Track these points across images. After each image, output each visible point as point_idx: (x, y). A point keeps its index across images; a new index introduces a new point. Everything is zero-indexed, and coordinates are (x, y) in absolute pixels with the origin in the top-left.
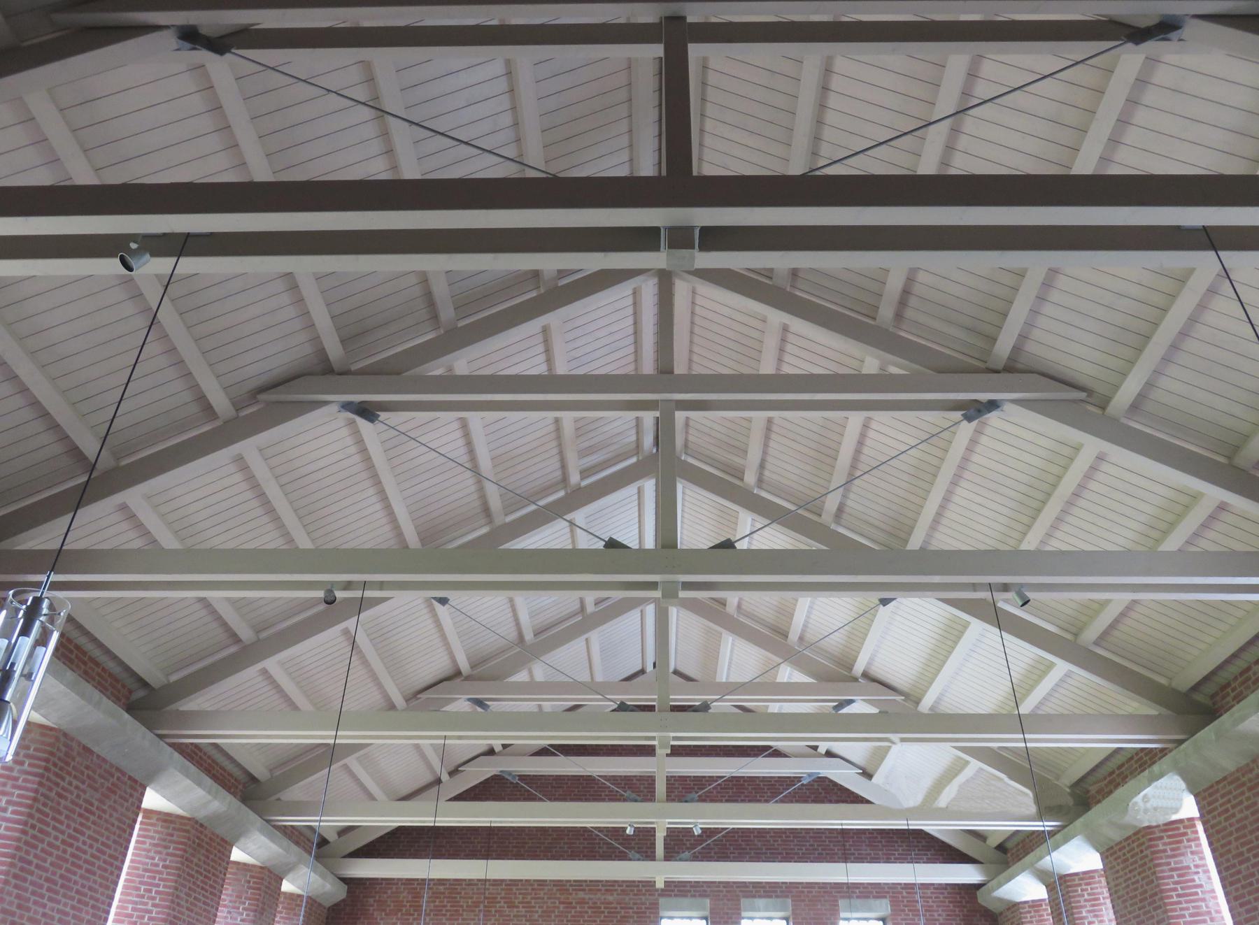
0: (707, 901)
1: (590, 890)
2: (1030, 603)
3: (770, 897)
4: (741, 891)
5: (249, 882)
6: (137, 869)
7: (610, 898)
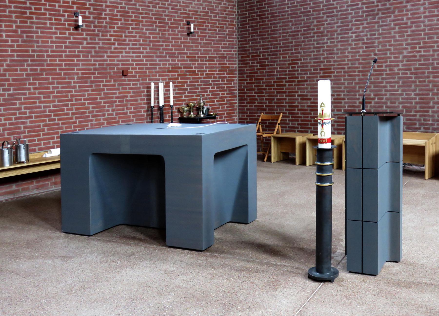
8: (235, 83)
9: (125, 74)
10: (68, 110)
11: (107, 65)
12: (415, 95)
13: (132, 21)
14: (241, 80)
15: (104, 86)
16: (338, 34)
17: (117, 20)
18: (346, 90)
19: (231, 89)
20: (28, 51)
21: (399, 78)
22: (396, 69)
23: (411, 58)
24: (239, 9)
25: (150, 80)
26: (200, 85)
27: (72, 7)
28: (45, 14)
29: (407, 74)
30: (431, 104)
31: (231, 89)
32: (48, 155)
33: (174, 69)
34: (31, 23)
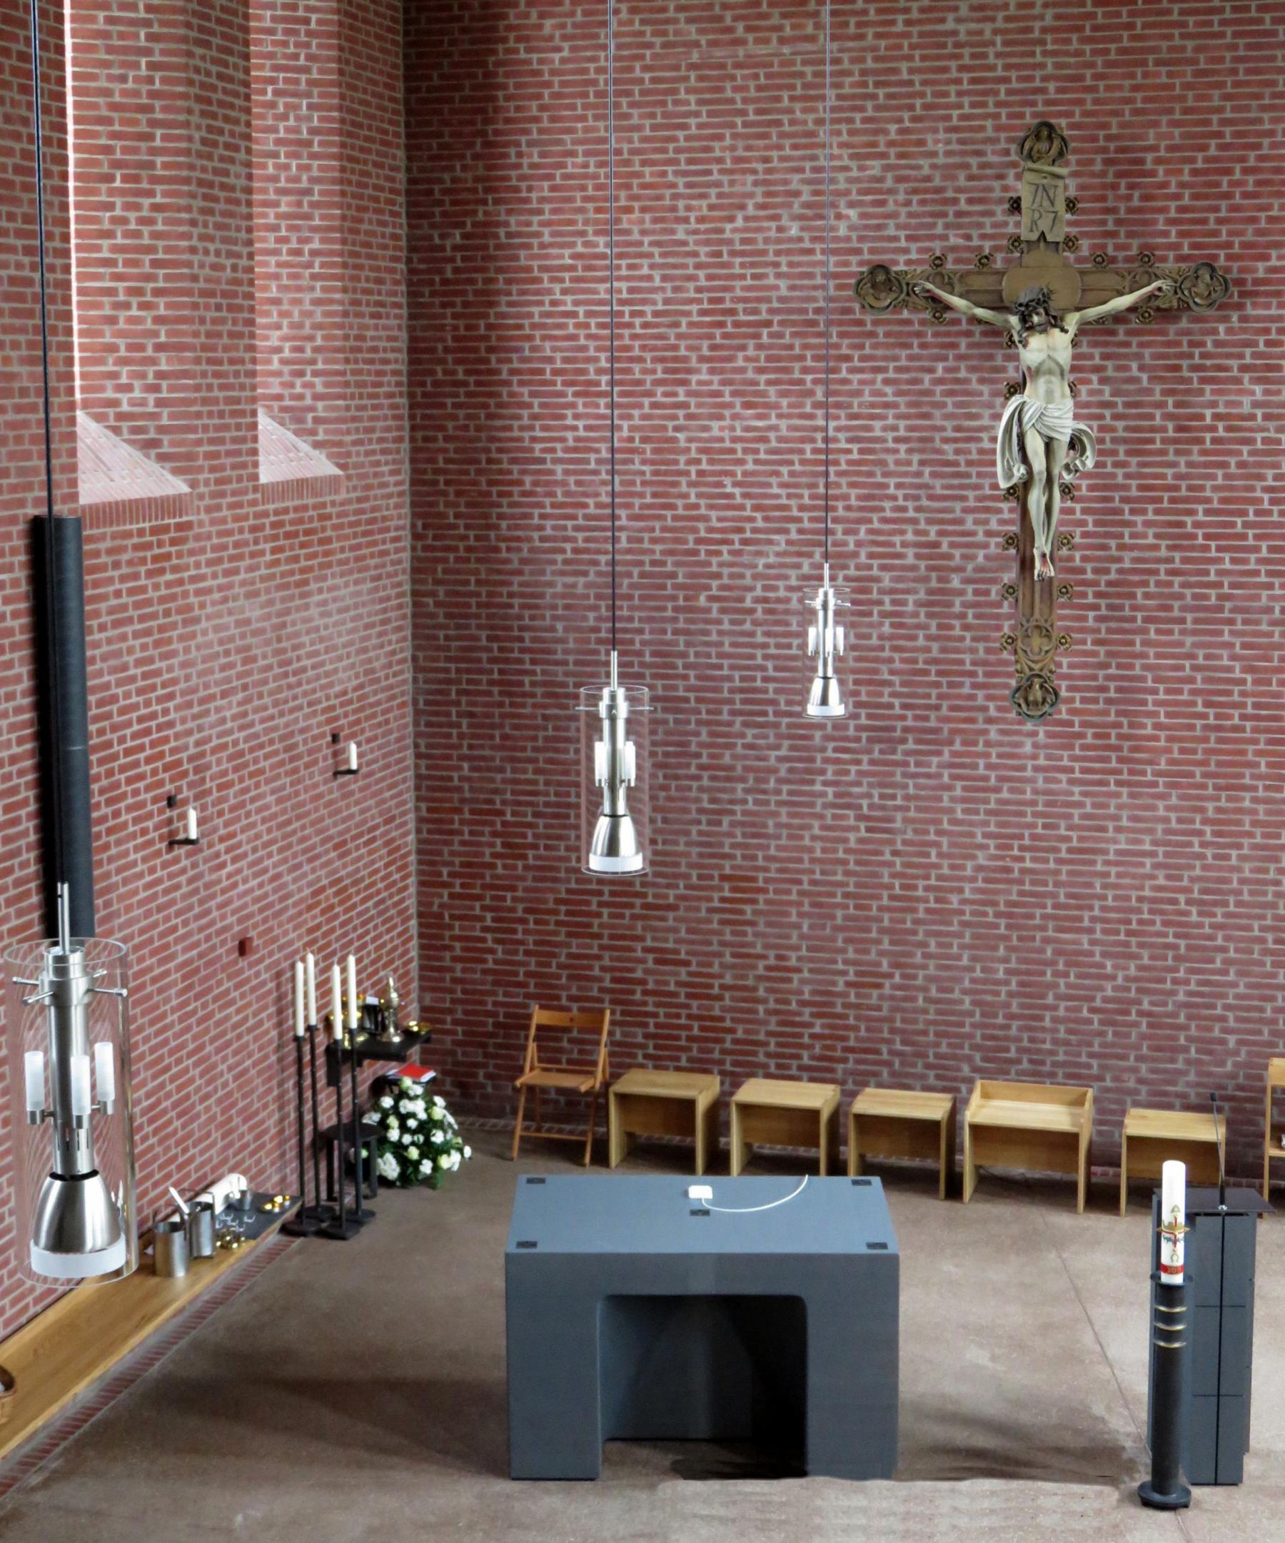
12: (1009, 972)
16: (780, 781)
21: (964, 924)
22: (954, 899)
30: (1050, 1000)
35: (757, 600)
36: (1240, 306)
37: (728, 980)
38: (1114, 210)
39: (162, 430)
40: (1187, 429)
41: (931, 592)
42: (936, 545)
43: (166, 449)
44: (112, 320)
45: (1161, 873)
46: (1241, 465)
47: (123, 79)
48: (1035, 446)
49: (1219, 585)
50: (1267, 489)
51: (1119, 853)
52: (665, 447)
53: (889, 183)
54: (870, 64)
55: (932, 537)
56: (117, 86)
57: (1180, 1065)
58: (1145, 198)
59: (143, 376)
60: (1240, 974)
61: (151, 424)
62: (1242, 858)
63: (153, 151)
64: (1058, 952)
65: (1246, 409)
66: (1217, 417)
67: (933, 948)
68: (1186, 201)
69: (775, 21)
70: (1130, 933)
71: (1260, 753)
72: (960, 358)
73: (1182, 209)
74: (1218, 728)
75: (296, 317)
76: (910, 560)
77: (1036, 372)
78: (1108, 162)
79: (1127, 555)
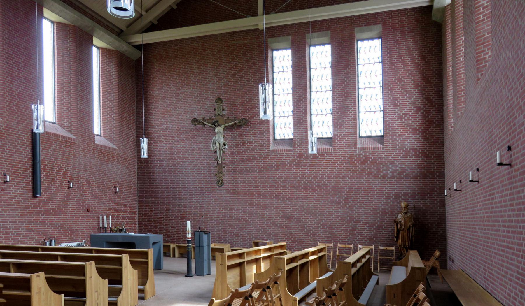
0: (290, 38)
1: (237, 40)
2: (30, 195)
3: (320, 31)
4: (306, 31)
5: (69, 31)
6: (60, 49)
7: (246, 42)
8: (137, 218)
9: (88, 210)
10: (66, 226)
11: (81, 206)
12: (221, 228)
13: (91, 185)
14: (139, 217)
15: (80, 216)
16: (188, 199)
17: (85, 185)
18: (11, 240)
19: (135, 221)
20: (50, 198)
21: (215, 221)
22: (213, 217)
23: (219, 213)
24: (138, 180)
25: (99, 214)
26: (120, 218)
27: (67, 178)
28: (56, 181)
29: (392, 180)
30: (227, 233)
31: (135, 221)
32: (60, 246)
33: (110, 209)
34: (52, 185)
35: (185, 172)
36: (250, 125)
37: (182, 230)
38: (232, 112)
39: (71, 129)
40: (244, 144)
41: (209, 170)
42: (209, 163)
43: (72, 132)
44: (63, 112)
45: (242, 212)
46: (251, 149)
47: (66, 78)
48: (217, 144)
49: (249, 167)
50: (255, 153)
51: (236, 209)
52: (172, 149)
53: (201, 109)
54: (198, 92)
55: (208, 161)
56: (65, 79)
57: (246, 243)
58: (236, 110)
59: (68, 121)
60: (254, 228)
61: (70, 128)
62: (254, 210)
63: (71, 89)
64: (228, 225)
65: (252, 141)
66: (248, 142)
67: (210, 225)
68: (242, 110)
69: (185, 86)
70: (238, 222)
71: (256, 193)
72: (212, 134)
73: (241, 111)
74: (250, 189)
75: (111, 125)
76: (205, 165)
77: (217, 133)
78: (231, 105)
79: (236, 163)
